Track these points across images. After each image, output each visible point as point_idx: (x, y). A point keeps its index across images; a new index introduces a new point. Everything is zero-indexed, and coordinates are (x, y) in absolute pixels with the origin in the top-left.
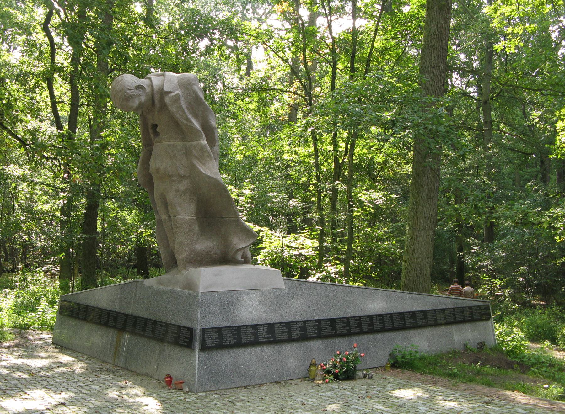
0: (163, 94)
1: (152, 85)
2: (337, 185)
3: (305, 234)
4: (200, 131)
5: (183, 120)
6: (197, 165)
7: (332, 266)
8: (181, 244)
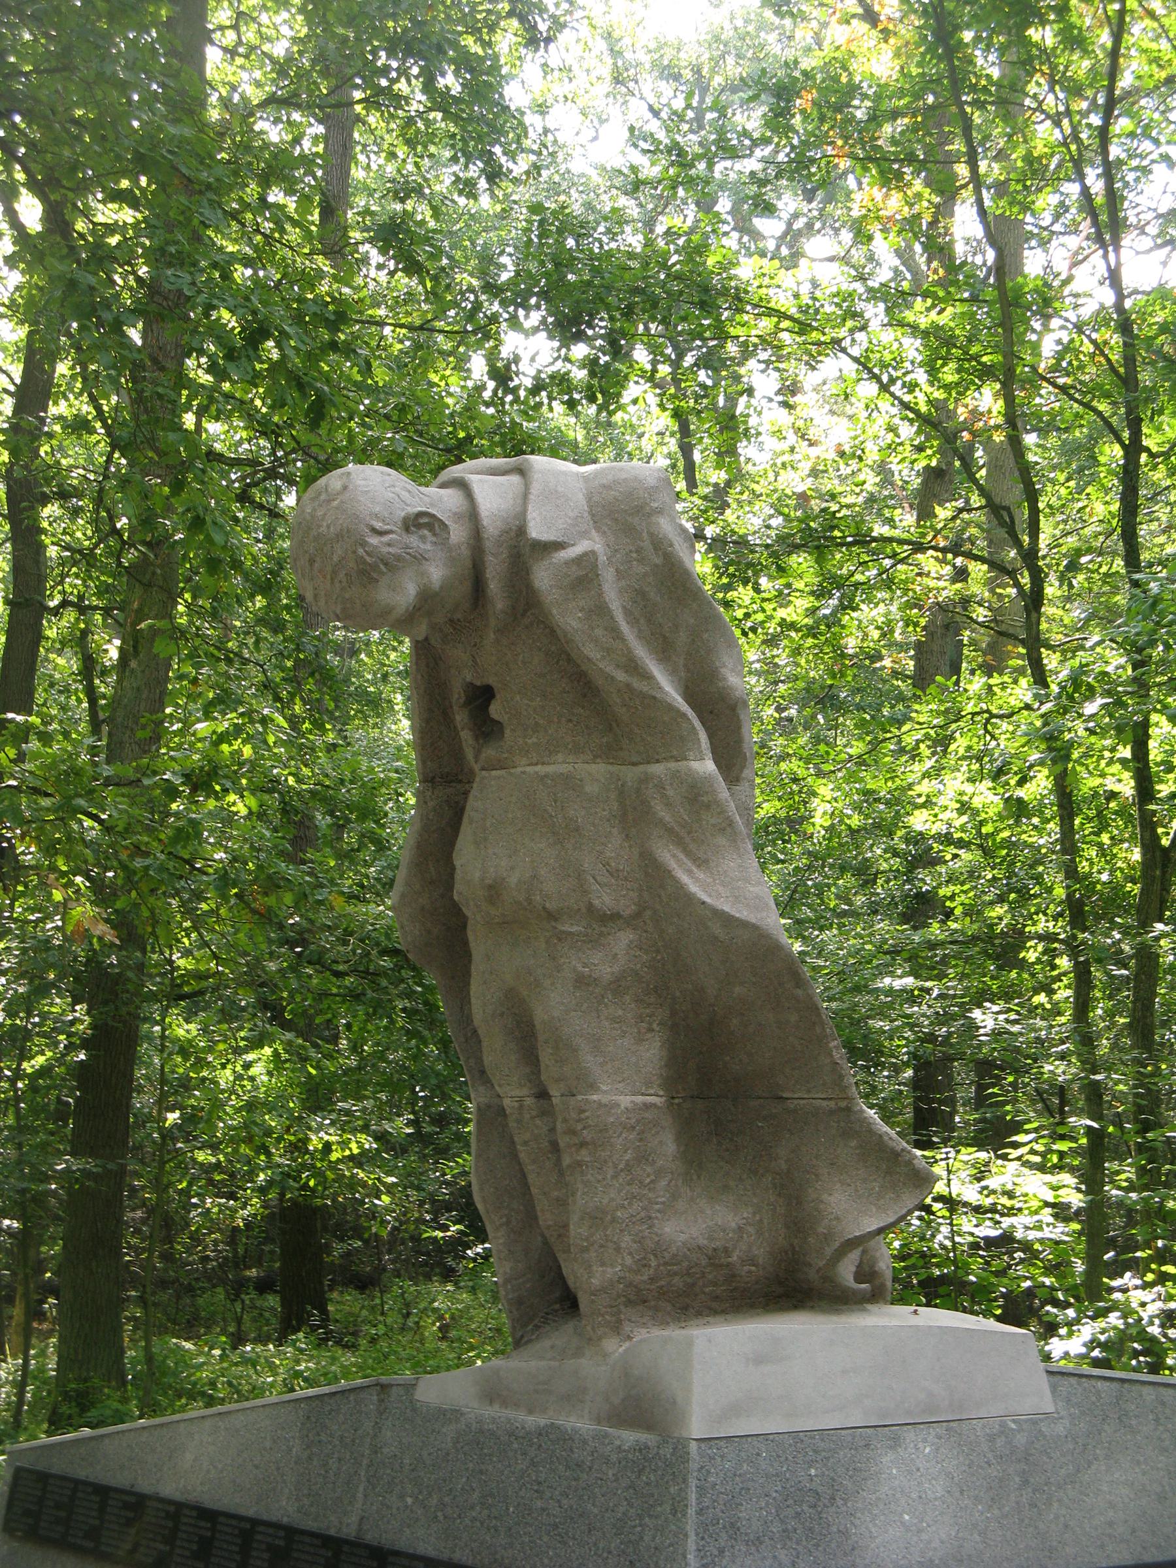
0: (523, 550)
1: (473, 514)
2: (1157, 939)
3: (1026, 1149)
4: (684, 715)
5: (610, 669)
6: (673, 864)
7: (1146, 1286)
8: (597, 1218)
